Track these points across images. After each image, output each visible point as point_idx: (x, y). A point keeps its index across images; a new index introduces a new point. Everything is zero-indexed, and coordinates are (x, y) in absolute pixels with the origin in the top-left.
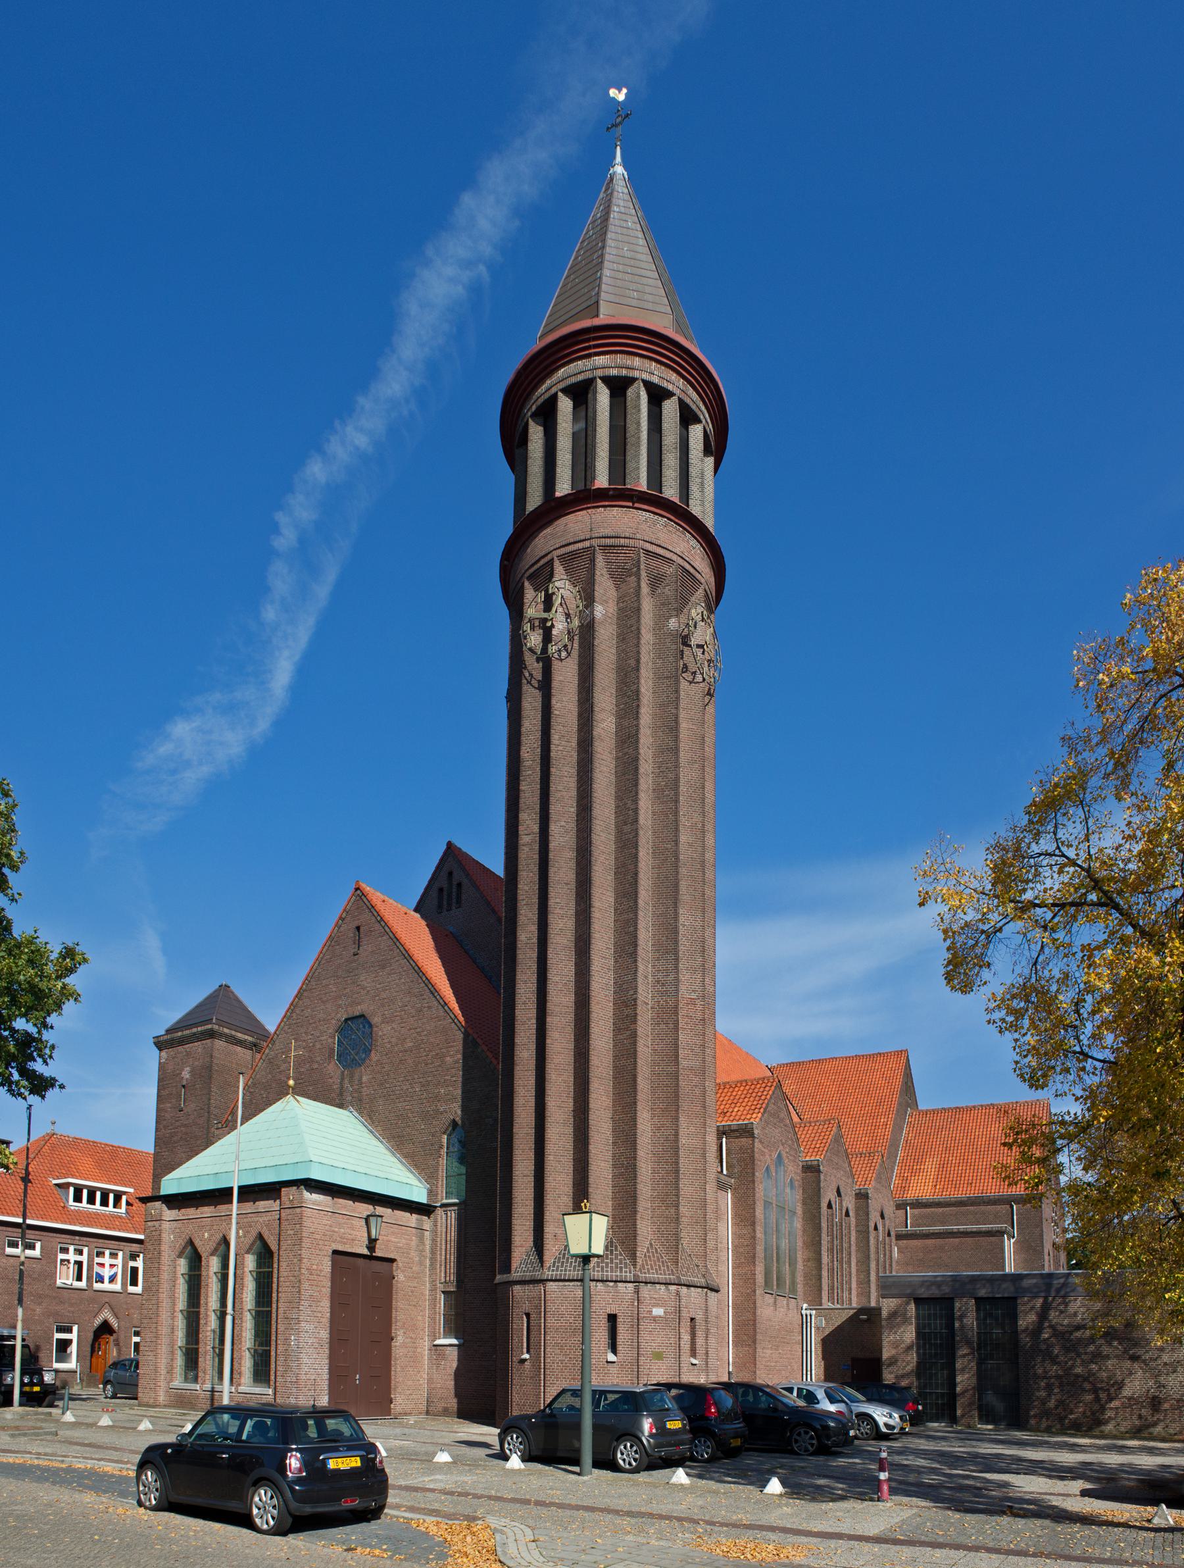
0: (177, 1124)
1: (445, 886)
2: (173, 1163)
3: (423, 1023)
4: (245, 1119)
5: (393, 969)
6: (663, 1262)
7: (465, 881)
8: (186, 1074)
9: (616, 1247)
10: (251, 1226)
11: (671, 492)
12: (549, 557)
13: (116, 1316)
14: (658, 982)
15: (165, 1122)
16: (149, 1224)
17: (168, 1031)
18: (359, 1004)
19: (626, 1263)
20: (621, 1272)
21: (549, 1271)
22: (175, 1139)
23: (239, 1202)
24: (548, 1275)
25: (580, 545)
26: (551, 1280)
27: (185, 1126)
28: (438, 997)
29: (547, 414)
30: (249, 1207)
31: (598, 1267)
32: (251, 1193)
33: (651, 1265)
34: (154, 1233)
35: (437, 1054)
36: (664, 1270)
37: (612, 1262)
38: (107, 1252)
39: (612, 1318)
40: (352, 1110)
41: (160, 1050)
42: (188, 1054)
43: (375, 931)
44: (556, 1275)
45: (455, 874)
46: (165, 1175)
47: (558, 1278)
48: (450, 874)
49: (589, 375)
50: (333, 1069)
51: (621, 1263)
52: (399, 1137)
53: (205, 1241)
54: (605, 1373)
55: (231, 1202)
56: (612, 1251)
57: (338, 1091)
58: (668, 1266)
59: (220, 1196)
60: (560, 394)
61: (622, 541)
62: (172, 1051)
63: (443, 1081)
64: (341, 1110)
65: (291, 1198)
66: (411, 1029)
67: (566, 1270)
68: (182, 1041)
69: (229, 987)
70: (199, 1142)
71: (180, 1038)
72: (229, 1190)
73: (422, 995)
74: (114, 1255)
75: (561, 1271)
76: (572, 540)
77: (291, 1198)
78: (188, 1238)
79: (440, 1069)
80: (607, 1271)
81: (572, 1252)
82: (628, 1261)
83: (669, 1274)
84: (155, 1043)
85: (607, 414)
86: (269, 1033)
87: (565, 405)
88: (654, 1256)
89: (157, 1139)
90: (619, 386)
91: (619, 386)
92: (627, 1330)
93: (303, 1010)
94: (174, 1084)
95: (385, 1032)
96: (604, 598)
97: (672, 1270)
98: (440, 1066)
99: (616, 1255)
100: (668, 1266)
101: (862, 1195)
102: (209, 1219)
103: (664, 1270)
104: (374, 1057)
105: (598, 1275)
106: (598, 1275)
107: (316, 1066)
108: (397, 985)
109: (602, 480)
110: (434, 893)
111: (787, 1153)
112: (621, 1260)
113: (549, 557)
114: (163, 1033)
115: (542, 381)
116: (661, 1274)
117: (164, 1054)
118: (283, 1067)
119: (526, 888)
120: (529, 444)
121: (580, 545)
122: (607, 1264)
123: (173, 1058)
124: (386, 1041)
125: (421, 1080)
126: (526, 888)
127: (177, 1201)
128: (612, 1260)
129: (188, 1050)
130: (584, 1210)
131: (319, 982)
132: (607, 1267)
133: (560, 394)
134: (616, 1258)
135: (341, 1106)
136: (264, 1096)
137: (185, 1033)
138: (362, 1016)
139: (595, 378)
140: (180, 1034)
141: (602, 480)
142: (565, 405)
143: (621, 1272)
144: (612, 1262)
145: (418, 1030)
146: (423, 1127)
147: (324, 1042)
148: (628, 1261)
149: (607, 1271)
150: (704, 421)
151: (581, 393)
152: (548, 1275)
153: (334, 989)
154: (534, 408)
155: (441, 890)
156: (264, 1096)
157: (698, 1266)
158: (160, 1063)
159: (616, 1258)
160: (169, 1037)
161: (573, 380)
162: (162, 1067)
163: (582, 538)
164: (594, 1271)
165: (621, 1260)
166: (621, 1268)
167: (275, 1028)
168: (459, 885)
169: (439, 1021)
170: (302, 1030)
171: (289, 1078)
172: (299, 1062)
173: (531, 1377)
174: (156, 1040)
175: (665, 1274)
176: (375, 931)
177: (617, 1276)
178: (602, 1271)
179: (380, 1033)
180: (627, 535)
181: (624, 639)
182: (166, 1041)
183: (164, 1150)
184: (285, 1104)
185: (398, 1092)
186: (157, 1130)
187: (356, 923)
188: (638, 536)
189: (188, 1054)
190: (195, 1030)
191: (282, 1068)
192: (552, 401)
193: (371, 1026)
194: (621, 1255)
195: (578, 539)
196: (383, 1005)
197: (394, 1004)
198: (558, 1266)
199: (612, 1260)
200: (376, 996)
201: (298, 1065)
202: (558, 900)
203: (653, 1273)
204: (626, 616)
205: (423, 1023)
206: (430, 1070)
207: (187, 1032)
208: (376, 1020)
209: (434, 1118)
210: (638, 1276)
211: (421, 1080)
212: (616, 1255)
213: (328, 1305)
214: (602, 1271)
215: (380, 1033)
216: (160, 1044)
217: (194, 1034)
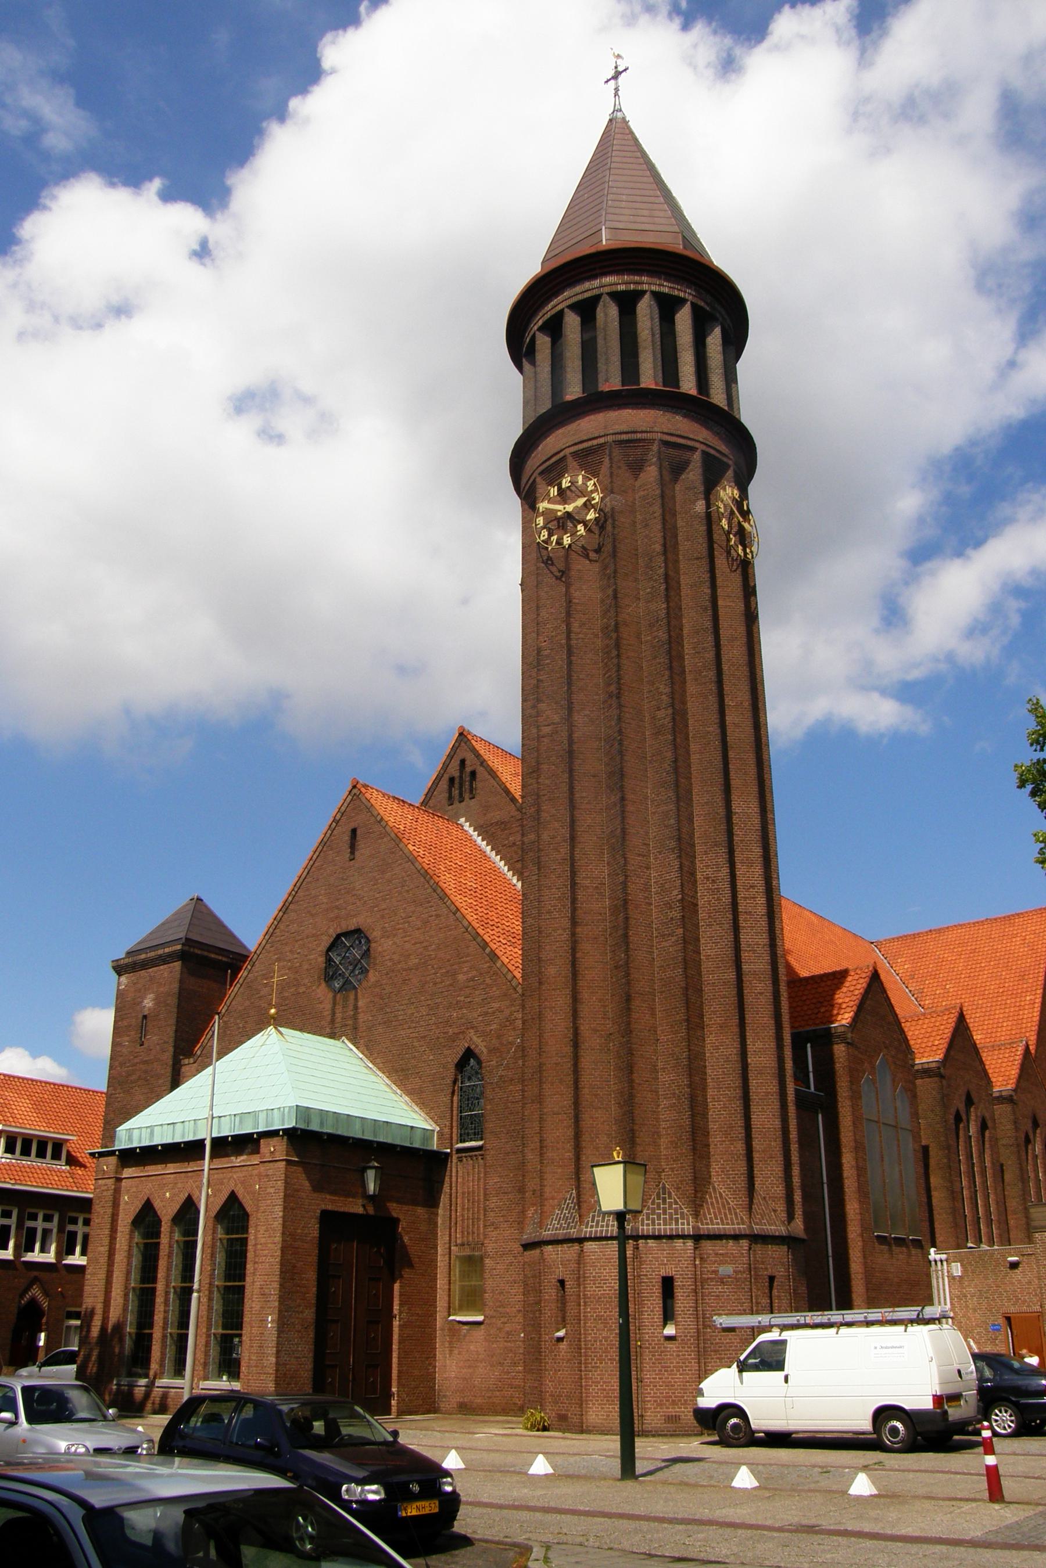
0: (137, 1060)
1: (457, 774)
2: (129, 1107)
3: (431, 937)
4: (222, 1054)
5: (395, 874)
6: (729, 1209)
7: (480, 771)
8: (148, 1003)
9: (670, 1194)
10: (222, 1184)
11: (688, 385)
12: (562, 454)
13: (46, 1294)
14: (708, 879)
15: (121, 1058)
16: (100, 1182)
17: (129, 954)
18: (355, 916)
19: (682, 1214)
20: (677, 1223)
21: (586, 1228)
22: (134, 1077)
23: (212, 1157)
24: (586, 1232)
25: (595, 442)
26: (590, 1239)
27: (145, 1062)
28: (296, 889)
29: (554, 327)
30: (221, 1163)
31: (648, 1219)
32: (224, 1146)
33: (715, 1213)
34: (105, 1193)
35: (448, 972)
36: (732, 1219)
37: (665, 1213)
38: (40, 1217)
39: (668, 1284)
40: (346, 1041)
41: (119, 974)
42: (152, 979)
43: (374, 832)
44: (596, 1232)
45: (468, 763)
46: (121, 1124)
47: (598, 1235)
48: (463, 762)
49: (596, 292)
50: (322, 992)
51: (676, 1214)
52: (403, 1070)
53: (167, 1208)
54: (661, 1352)
55: (204, 1159)
56: (664, 1200)
57: (329, 1018)
58: (736, 1214)
59: (190, 1150)
60: (566, 310)
61: (639, 436)
62: (133, 976)
63: (455, 1002)
64: (332, 1041)
65: (272, 1149)
66: (416, 943)
67: (607, 1226)
68: (145, 965)
69: (202, 900)
70: (161, 1081)
71: (144, 960)
72: (201, 1143)
73: (429, 902)
74: (48, 1218)
75: (602, 1226)
76: (585, 438)
77: (272, 1149)
78: (146, 1199)
79: (451, 988)
80: (659, 1224)
81: (603, 1209)
82: (685, 1211)
83: (738, 1224)
84: (114, 968)
85: (617, 323)
86: (250, 952)
87: (572, 322)
88: (718, 1202)
89: (111, 1079)
90: (627, 302)
91: (627, 302)
92: (687, 1296)
93: (288, 926)
94: (134, 1015)
95: (384, 947)
96: (623, 489)
97: (742, 1219)
98: (451, 985)
99: (670, 1204)
100: (736, 1214)
101: (1005, 1099)
102: (172, 1176)
103: (732, 1219)
104: (373, 976)
105: (648, 1230)
106: (648, 1230)
107: (302, 990)
108: (400, 893)
109: (611, 380)
110: (444, 784)
111: (893, 1057)
112: (676, 1210)
113: (562, 454)
114: (124, 956)
115: (549, 299)
116: (728, 1224)
117: (123, 979)
118: (265, 991)
119: (547, 782)
120: (537, 354)
121: (595, 442)
122: (659, 1215)
123: (135, 984)
124: (387, 958)
125: (429, 1002)
126: (547, 782)
127: (131, 1157)
128: (665, 1210)
129: (152, 974)
130: (617, 1159)
131: (307, 893)
132: (659, 1219)
133: (566, 310)
134: (670, 1207)
135: (332, 1036)
136: (241, 1025)
137: (149, 955)
138: (358, 931)
139: (602, 294)
140: (143, 956)
141: (611, 380)
142: (572, 322)
143: (677, 1223)
144: (665, 1213)
145: (425, 944)
146: (431, 1057)
147: (313, 962)
148: (685, 1211)
149: (659, 1224)
150: (721, 319)
151: (587, 309)
152: (586, 1232)
153: (325, 901)
154: (540, 323)
155: (452, 780)
156: (241, 1025)
157: (775, 1211)
158: (118, 990)
159: (670, 1207)
160: (130, 960)
161: (580, 297)
162: (120, 995)
163: (596, 435)
164: (643, 1225)
165: (676, 1210)
166: (677, 1220)
167: (256, 946)
168: (473, 774)
169: (450, 930)
170: (287, 949)
171: (271, 1006)
172: (283, 987)
173: (569, 1360)
174: (115, 964)
175: (733, 1224)
176: (374, 832)
177: (671, 1229)
178: (653, 1223)
179: (380, 949)
180: (644, 429)
181: (647, 525)
182: (127, 965)
183: (118, 1091)
184: (265, 1037)
185: (401, 1018)
186: (111, 1068)
187: (352, 825)
188: (656, 429)
189: (152, 979)
190: (160, 952)
191: (262, 993)
192: (559, 317)
193: (368, 941)
194: (676, 1203)
195: (591, 436)
196: (383, 917)
197: (396, 915)
198: (598, 1222)
199: (665, 1210)
200: (374, 907)
201: (281, 991)
202: (584, 794)
203: (718, 1224)
204: (647, 503)
205: (431, 937)
206: (440, 990)
207: (152, 954)
208: (375, 934)
209: (444, 1046)
210: (699, 1228)
211: (429, 1002)
212: (670, 1204)
213: (315, 1277)
214: (653, 1223)
215: (380, 949)
216: (120, 969)
217: (160, 956)
